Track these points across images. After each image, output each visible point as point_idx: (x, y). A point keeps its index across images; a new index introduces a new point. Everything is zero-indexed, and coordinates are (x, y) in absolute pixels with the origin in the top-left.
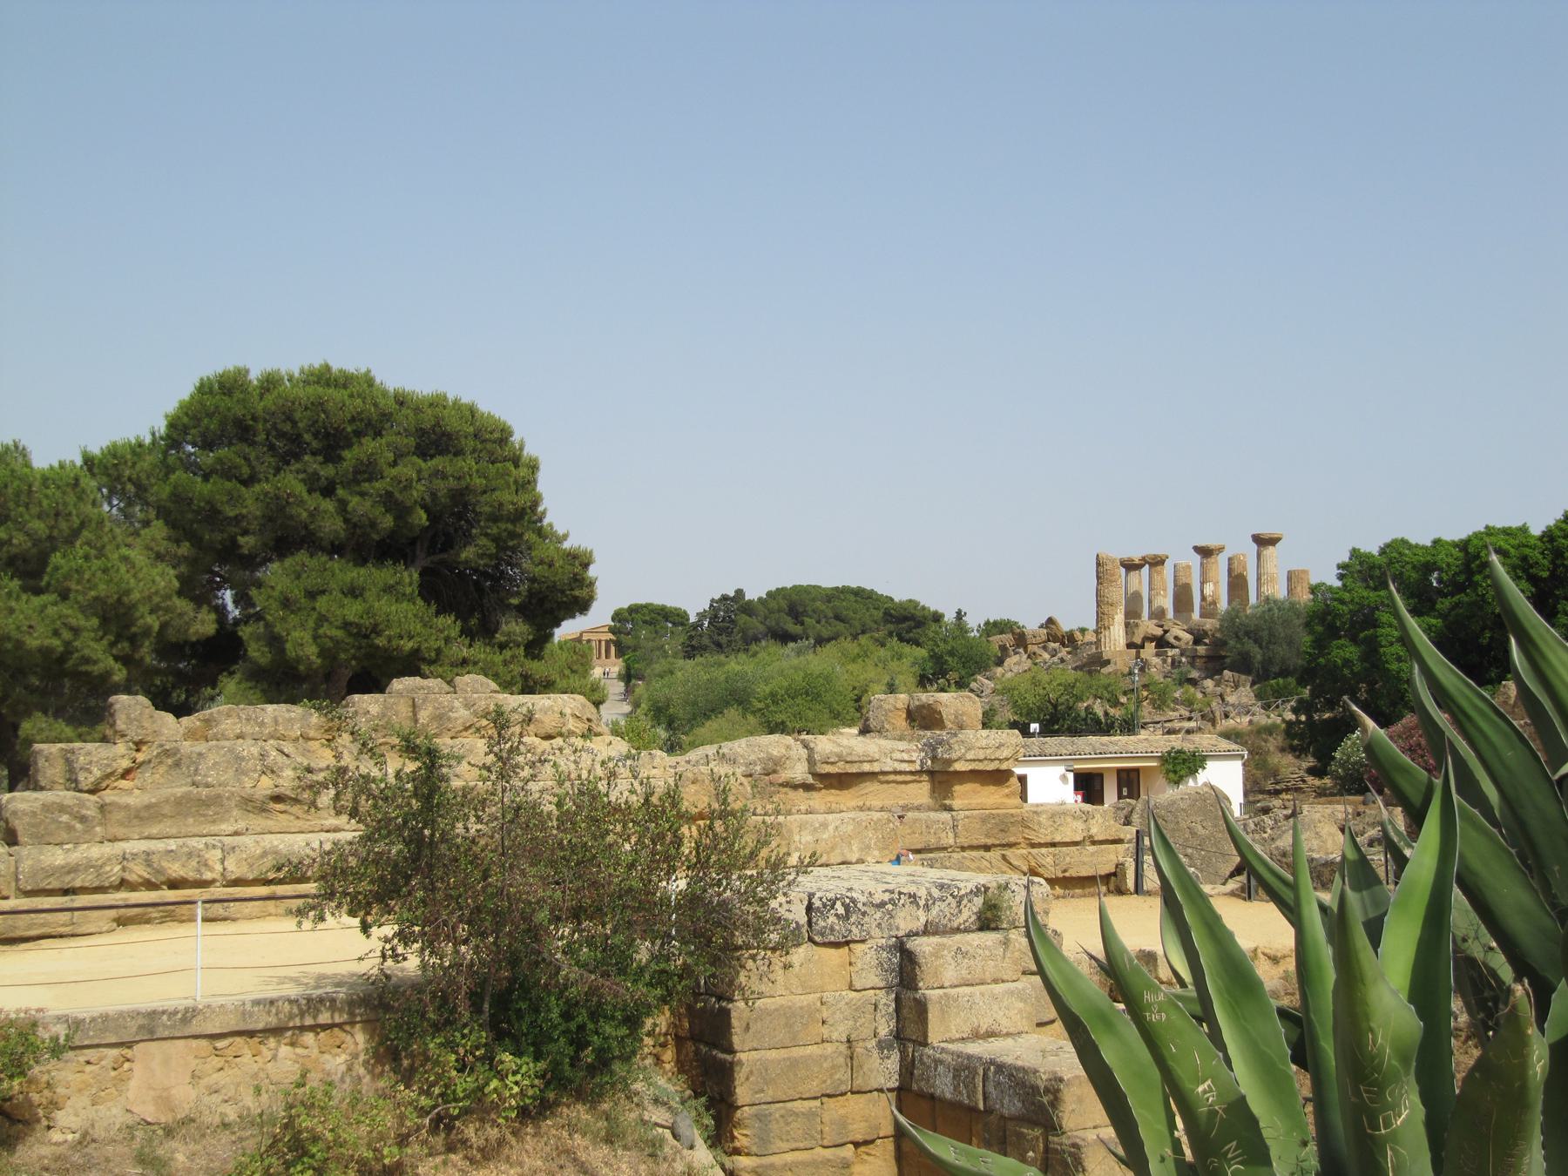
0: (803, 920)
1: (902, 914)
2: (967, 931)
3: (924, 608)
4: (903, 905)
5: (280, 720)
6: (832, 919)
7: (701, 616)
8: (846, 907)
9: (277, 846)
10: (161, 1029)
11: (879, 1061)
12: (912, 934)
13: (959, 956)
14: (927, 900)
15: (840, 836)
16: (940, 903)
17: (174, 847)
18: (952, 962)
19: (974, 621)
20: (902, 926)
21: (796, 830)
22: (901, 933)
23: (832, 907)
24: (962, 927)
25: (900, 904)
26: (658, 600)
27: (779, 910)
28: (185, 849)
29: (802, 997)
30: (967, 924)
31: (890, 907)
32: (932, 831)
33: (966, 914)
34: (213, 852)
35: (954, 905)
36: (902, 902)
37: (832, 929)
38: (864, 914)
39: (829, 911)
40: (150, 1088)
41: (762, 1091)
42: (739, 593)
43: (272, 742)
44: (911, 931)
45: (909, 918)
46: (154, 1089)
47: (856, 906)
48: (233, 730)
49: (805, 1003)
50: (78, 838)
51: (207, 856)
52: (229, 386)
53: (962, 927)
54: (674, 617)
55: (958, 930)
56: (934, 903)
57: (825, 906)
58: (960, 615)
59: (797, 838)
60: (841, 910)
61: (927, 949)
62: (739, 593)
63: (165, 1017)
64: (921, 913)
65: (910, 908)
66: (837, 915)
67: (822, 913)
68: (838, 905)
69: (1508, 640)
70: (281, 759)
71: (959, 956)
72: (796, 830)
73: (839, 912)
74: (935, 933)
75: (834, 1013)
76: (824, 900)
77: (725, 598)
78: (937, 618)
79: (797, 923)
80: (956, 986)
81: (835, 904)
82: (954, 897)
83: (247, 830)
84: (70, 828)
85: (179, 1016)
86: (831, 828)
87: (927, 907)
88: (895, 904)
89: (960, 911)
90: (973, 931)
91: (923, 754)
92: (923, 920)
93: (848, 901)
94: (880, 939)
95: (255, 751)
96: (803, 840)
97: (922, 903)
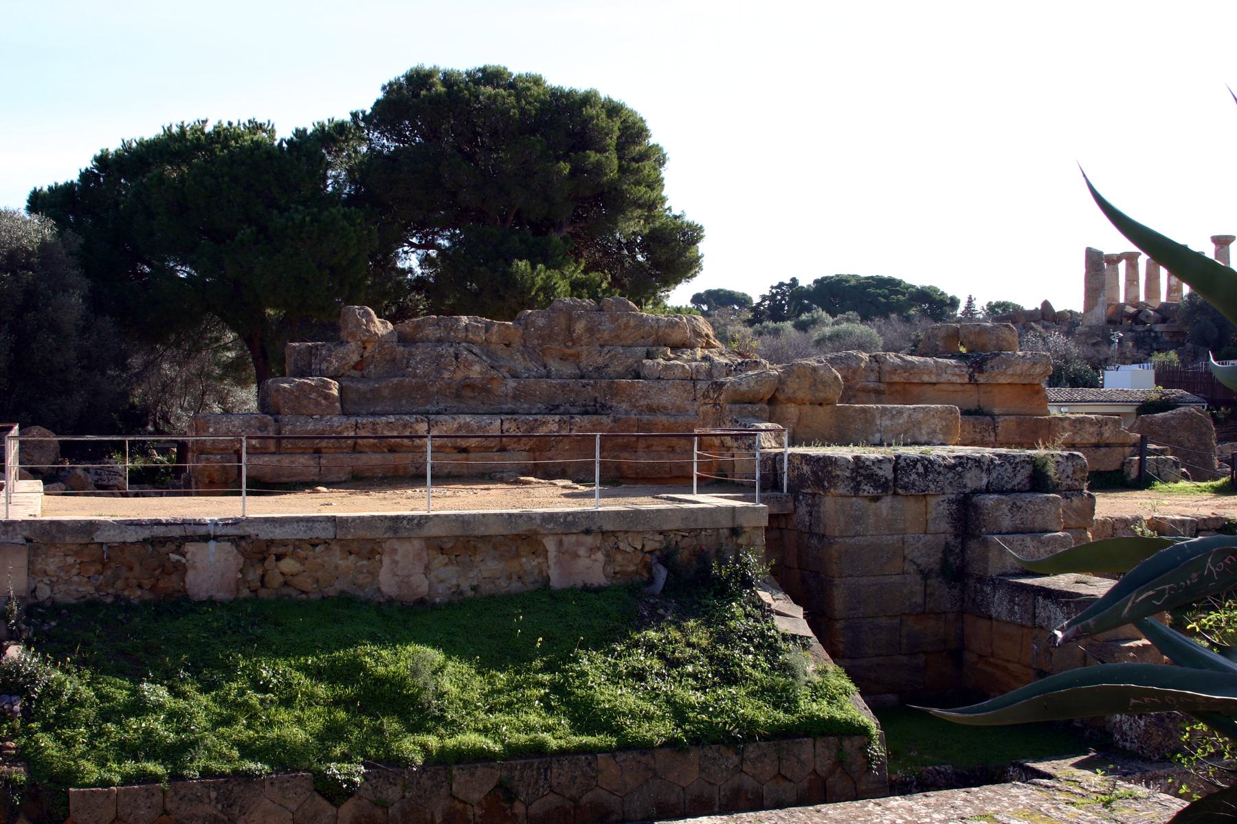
0: (891, 476)
1: (969, 475)
2: (1020, 491)
3: (943, 294)
4: (970, 468)
5: (470, 329)
6: (914, 476)
7: (764, 298)
8: (925, 468)
9: (469, 423)
10: (403, 531)
11: (947, 590)
12: (976, 492)
13: (1015, 509)
14: (989, 465)
15: (912, 422)
16: (999, 468)
17: (393, 420)
18: (1009, 514)
19: (980, 305)
20: (969, 485)
21: (878, 416)
22: (967, 491)
23: (914, 466)
24: (1016, 488)
25: (968, 467)
26: (729, 287)
27: (873, 467)
28: (401, 422)
29: (889, 537)
30: (1020, 486)
31: (959, 469)
32: (978, 430)
33: (1019, 478)
34: (422, 425)
35: (1010, 470)
36: (969, 465)
37: (914, 484)
38: (939, 473)
39: (912, 470)
40: (395, 575)
41: (856, 609)
42: (794, 280)
43: (464, 344)
44: (975, 489)
45: (974, 478)
46: (397, 576)
47: (933, 467)
48: (434, 334)
49: (890, 542)
50: (323, 410)
51: (417, 428)
52: (418, 79)
53: (1016, 488)
54: (743, 300)
55: (1013, 491)
56: (994, 468)
57: (908, 465)
58: (970, 301)
59: (878, 422)
60: (921, 470)
61: (990, 503)
62: (794, 280)
63: (405, 522)
64: (984, 475)
65: (975, 471)
66: (917, 473)
67: (906, 471)
68: (919, 465)
69: (1028, 767)
70: (471, 357)
71: (1015, 509)
72: (878, 416)
73: (920, 471)
74: (995, 492)
75: (913, 551)
76: (908, 461)
77: (781, 285)
78: (954, 303)
79: (886, 478)
80: (1012, 533)
81: (916, 464)
82: (1011, 464)
83: (446, 410)
84: (318, 404)
85: (416, 521)
86: (905, 415)
87: (989, 471)
88: (963, 467)
89: (1015, 475)
90: (1025, 492)
91: (971, 370)
92: (985, 481)
93: (926, 462)
94: (951, 494)
95: (451, 350)
96: (883, 425)
97: (985, 467)
